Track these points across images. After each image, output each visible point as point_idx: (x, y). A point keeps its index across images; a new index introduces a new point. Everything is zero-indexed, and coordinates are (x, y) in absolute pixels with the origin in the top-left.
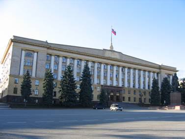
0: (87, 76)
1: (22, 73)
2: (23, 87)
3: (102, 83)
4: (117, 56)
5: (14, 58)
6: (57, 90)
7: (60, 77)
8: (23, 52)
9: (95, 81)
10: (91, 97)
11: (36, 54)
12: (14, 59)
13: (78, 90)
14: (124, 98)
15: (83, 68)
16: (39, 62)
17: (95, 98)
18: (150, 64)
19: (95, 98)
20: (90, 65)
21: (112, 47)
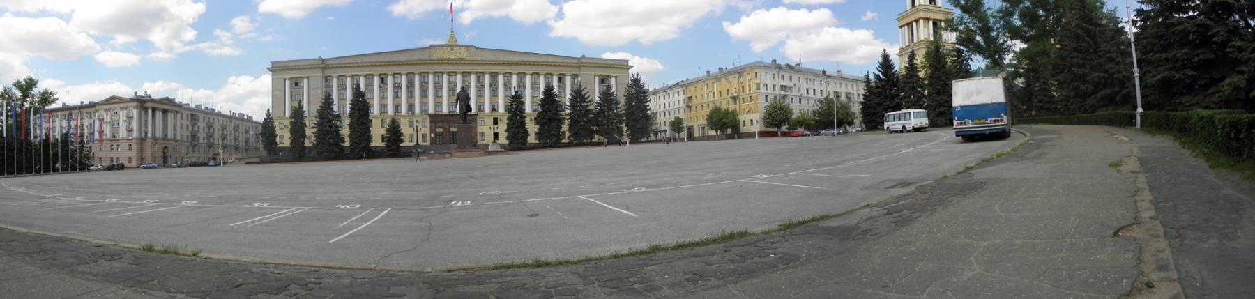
0: (361, 106)
1: (288, 114)
2: (509, 109)
3: (431, 111)
4: (463, 54)
5: (275, 93)
6: (309, 131)
7: (566, 98)
8: (287, 81)
9: (375, 110)
10: (369, 137)
11: (305, 81)
12: (275, 95)
13: (1210, 33)
14: (482, 134)
15: (542, 89)
16: (312, 92)
17: (377, 142)
18: (551, 60)
19: (377, 142)
20: (555, 83)
21: (453, 37)
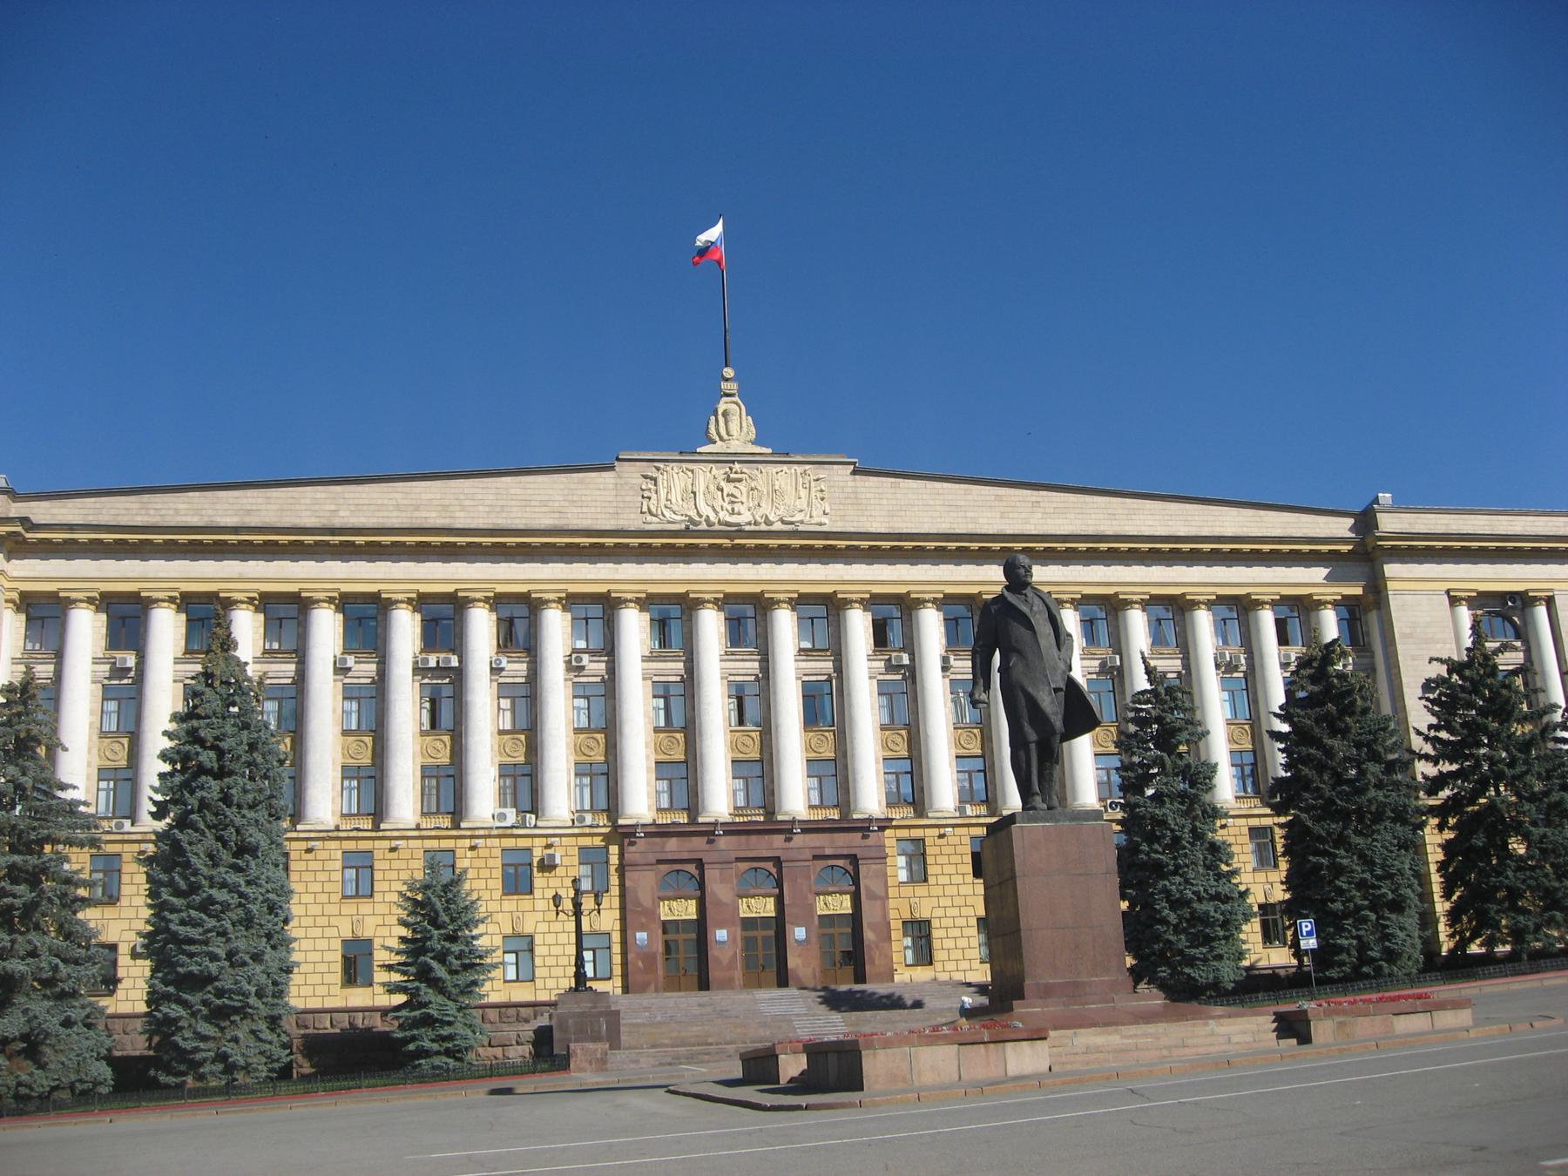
11: (1541, 612)
